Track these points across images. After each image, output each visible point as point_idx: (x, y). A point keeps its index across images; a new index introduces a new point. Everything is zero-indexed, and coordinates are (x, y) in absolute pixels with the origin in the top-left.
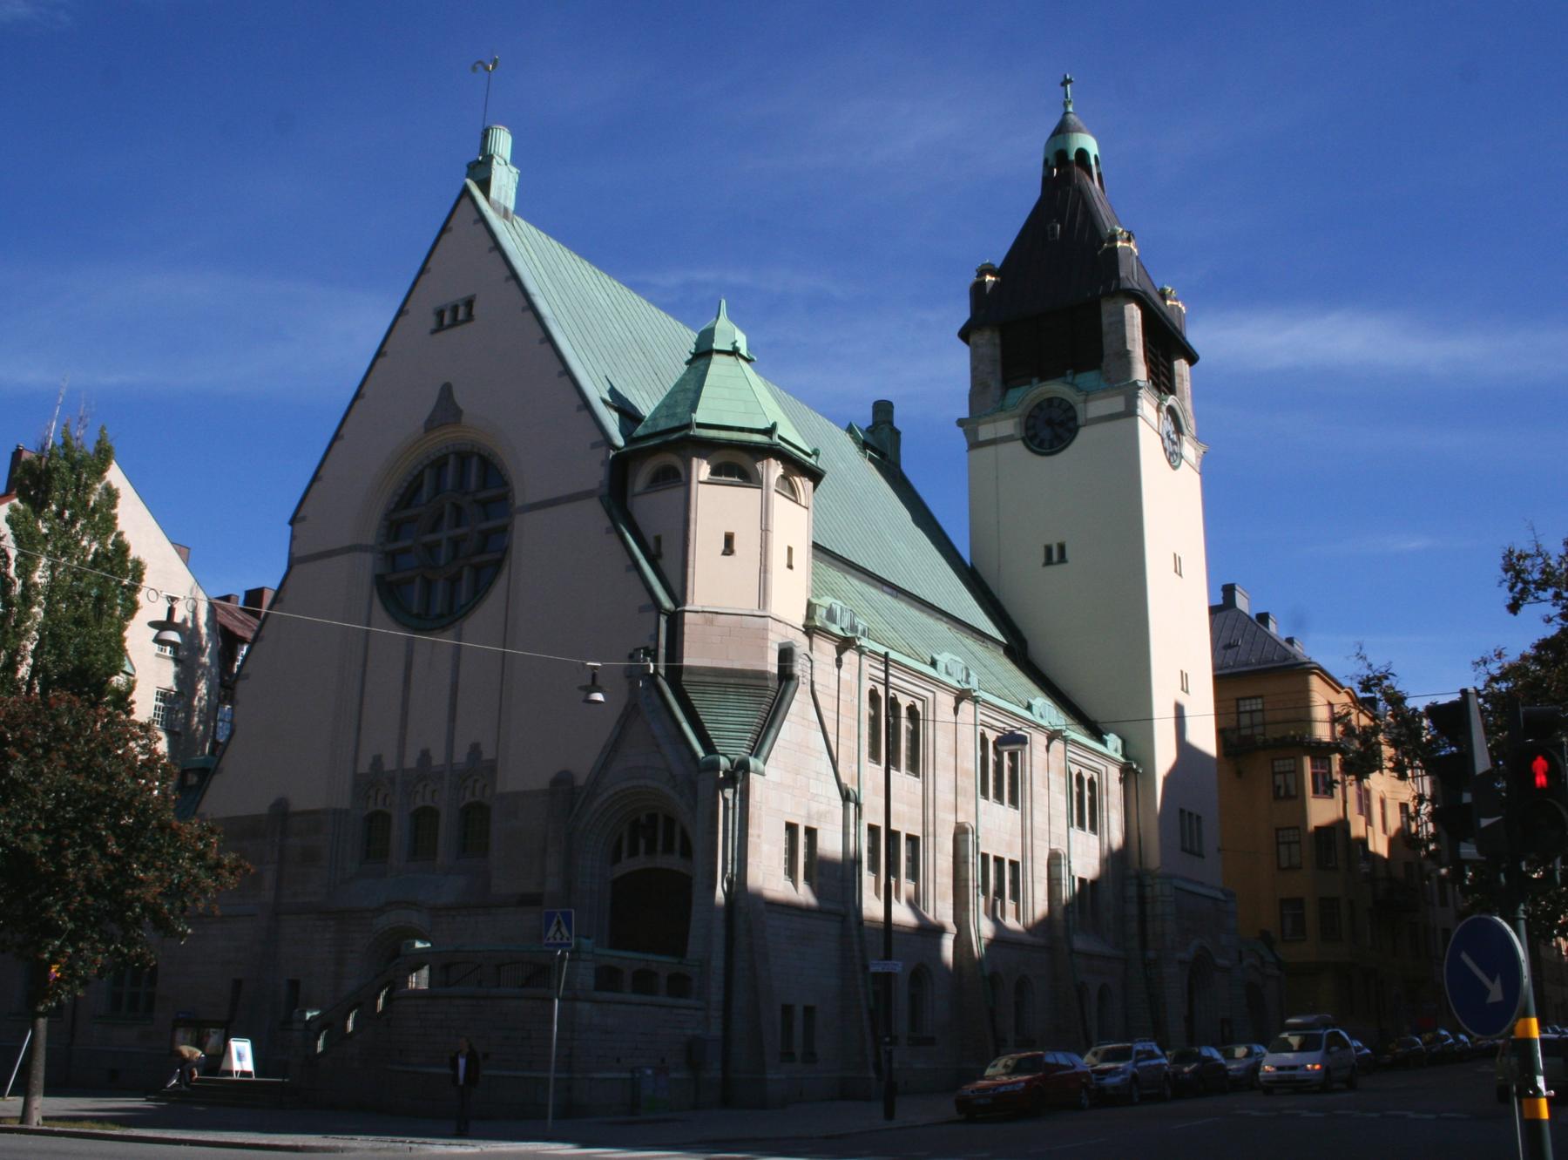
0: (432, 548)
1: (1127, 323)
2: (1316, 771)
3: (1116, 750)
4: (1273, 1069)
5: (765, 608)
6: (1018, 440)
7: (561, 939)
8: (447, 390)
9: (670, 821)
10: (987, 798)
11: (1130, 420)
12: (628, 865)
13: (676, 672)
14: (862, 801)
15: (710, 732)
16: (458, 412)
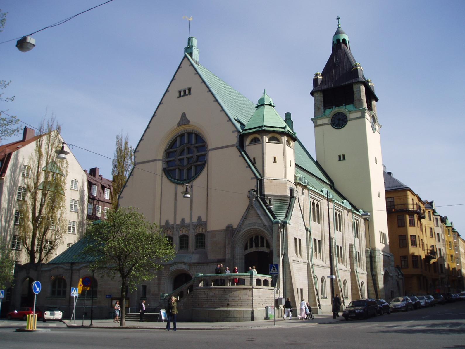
0: (181, 160)
1: (361, 91)
2: (410, 219)
4: (285, 315)
5: (286, 178)
6: (329, 124)
7: (275, 272)
8: (184, 115)
9: (262, 238)
11: (364, 119)
12: (249, 250)
13: (262, 195)
14: (311, 231)
15: (274, 213)
16: (188, 122)
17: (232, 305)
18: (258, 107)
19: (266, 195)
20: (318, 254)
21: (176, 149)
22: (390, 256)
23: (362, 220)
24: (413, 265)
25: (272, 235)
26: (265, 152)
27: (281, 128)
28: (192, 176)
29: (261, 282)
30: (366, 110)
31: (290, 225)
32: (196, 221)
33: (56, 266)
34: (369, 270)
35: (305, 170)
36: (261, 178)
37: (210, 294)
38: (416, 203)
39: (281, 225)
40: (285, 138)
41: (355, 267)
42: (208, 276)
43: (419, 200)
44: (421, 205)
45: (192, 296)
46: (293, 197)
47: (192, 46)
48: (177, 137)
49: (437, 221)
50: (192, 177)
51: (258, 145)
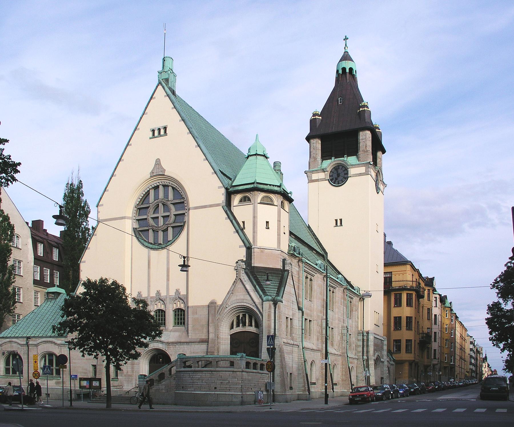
12: (236, 330)
31: (282, 302)
33: (8, 340)
43: (419, 276)
44: (421, 281)
50: (169, 241)
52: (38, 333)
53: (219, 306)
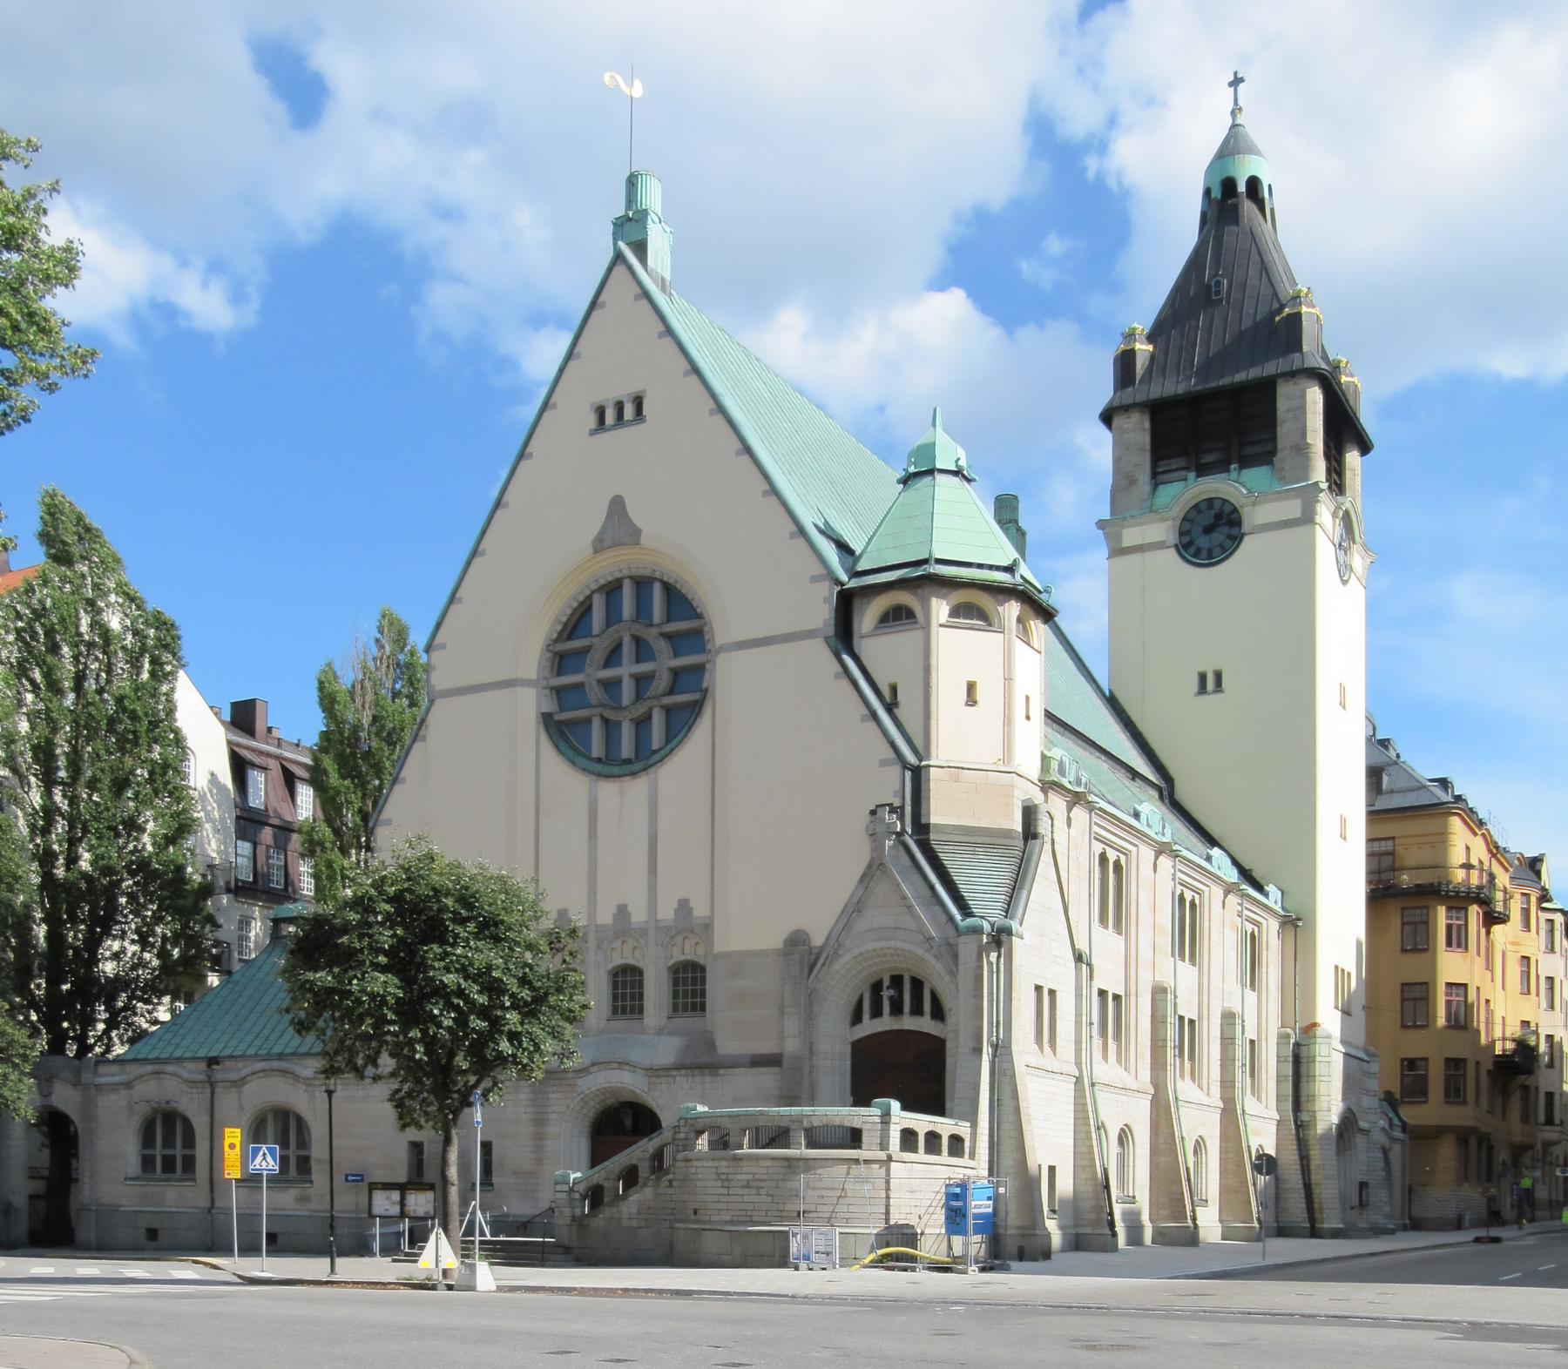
0: (611, 686)
3: (1276, 902)
8: (617, 506)
9: (917, 984)
10: (1183, 960)
12: (869, 1027)
13: (922, 828)
16: (636, 534)
17: (814, 1215)
18: (906, 480)
19: (936, 825)
20: (1112, 1046)
21: (588, 644)
22: (1366, 1058)
23: (1274, 925)
24: (1447, 1095)
25: (953, 974)
26: (933, 662)
27: (998, 568)
28: (655, 746)
29: (917, 1141)
30: (1322, 491)
32: (671, 915)
33: (150, 1068)
34: (1289, 1105)
35: (1069, 731)
36: (918, 763)
37: (739, 1177)
38: (1481, 862)
39: (991, 938)
40: (1012, 609)
41: (1238, 1092)
42: (730, 1116)
43: (1490, 851)
44: (1497, 869)
45: (670, 1181)
46: (1035, 836)
47: (645, 213)
48: (593, 592)
49: (1551, 931)
50: (655, 752)
51: (904, 633)
52: (243, 1047)
53: (816, 951)
